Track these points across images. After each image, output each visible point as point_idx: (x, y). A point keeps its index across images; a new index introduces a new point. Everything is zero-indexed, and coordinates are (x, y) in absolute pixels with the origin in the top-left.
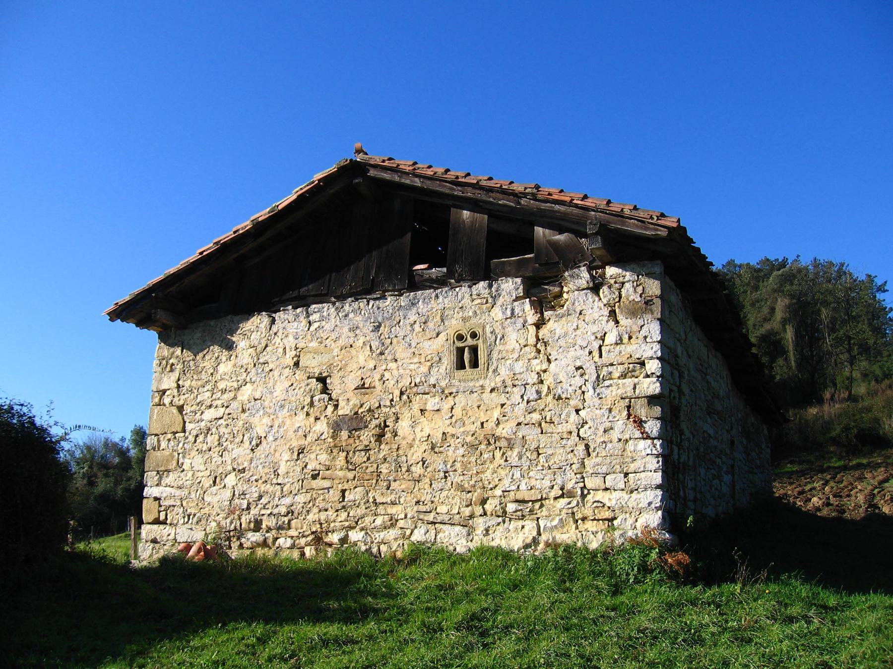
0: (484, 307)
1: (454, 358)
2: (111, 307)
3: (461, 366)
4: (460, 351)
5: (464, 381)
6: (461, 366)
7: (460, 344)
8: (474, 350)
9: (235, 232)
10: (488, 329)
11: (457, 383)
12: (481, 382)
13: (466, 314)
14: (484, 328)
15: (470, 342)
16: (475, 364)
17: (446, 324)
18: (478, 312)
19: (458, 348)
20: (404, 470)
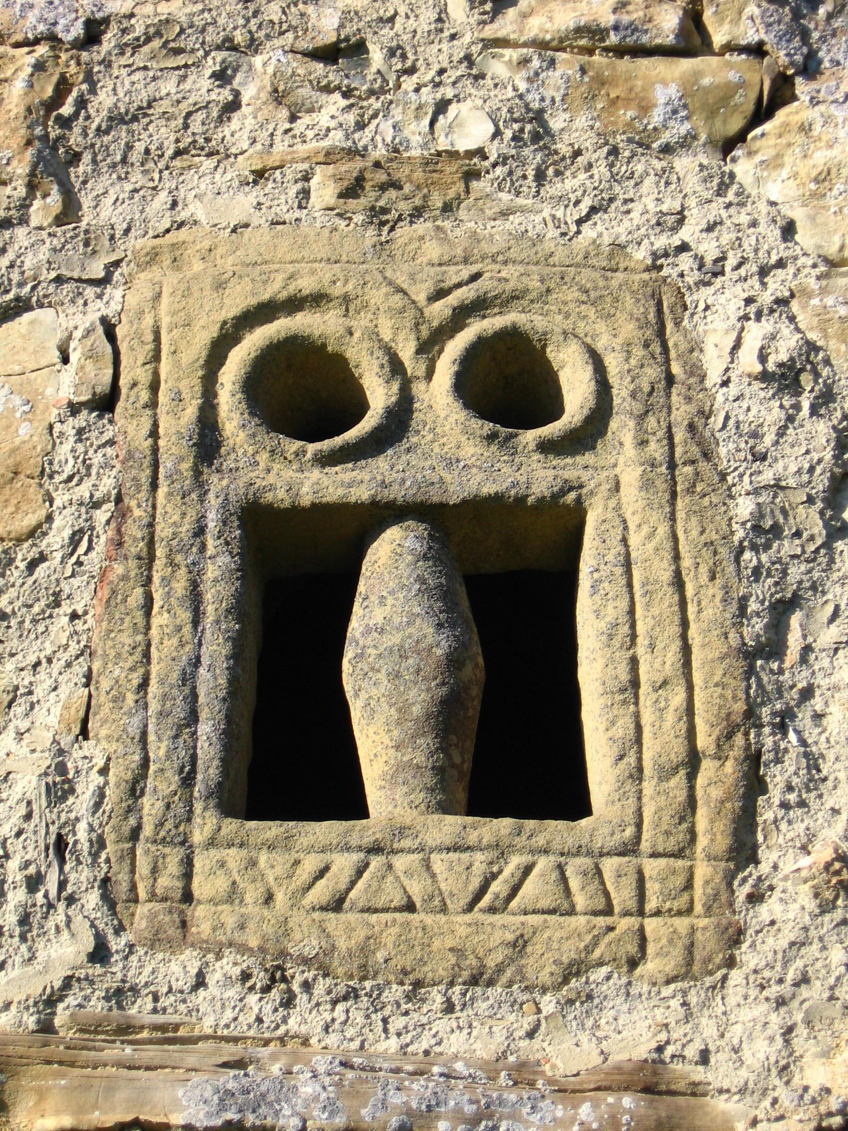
0: (665, 80)
1: (194, 639)
2: (798, 224)
3: (288, 757)
4: (294, 583)
5: (357, 981)
6: (288, 757)
7: (300, 477)
8: (513, 591)
9: (33, 51)
10: (724, 337)
11: (223, 1005)
12: (631, 1028)
13: (401, 127)
14: (662, 317)
15: (453, 450)
16: (515, 747)
17: (106, 203)
18: (572, 127)
19: (263, 529)
20: (120, 597)
